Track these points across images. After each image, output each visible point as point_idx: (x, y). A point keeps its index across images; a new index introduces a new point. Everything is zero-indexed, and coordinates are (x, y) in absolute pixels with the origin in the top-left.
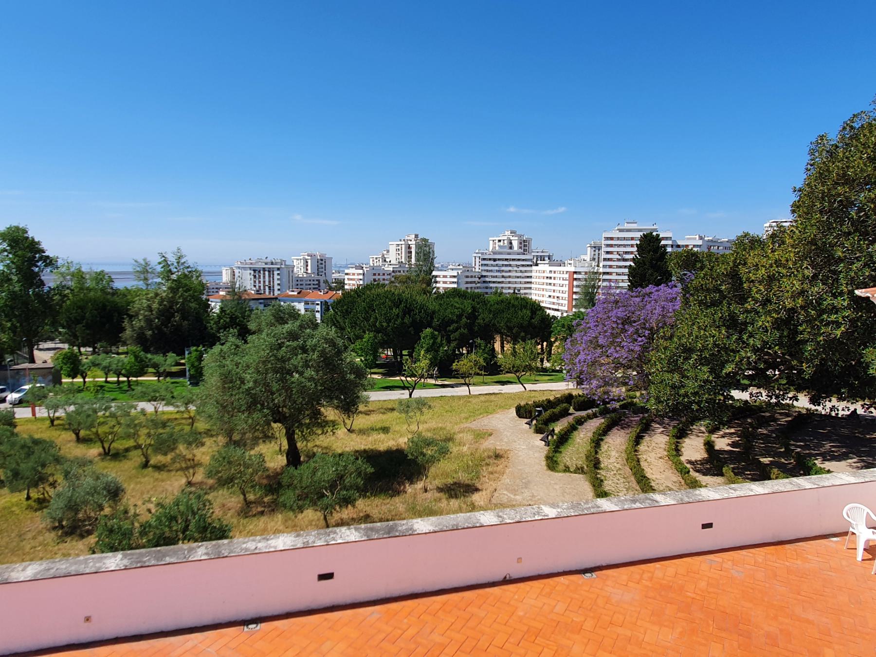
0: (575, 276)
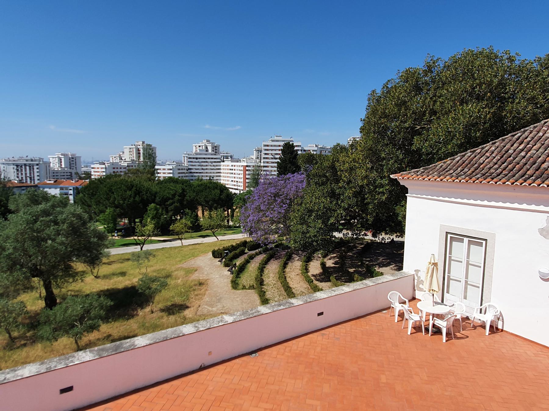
0: (247, 168)
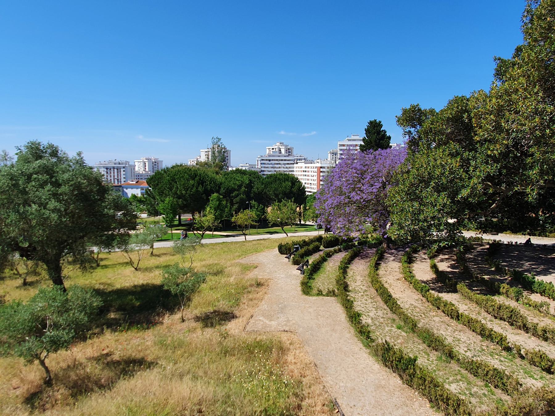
0: (321, 170)
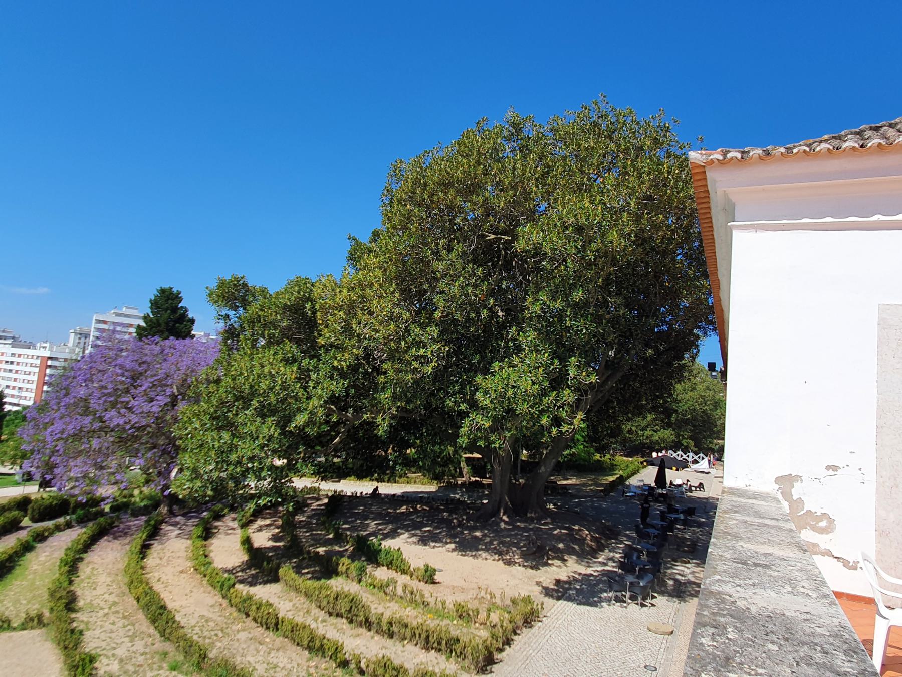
0: (49, 363)
